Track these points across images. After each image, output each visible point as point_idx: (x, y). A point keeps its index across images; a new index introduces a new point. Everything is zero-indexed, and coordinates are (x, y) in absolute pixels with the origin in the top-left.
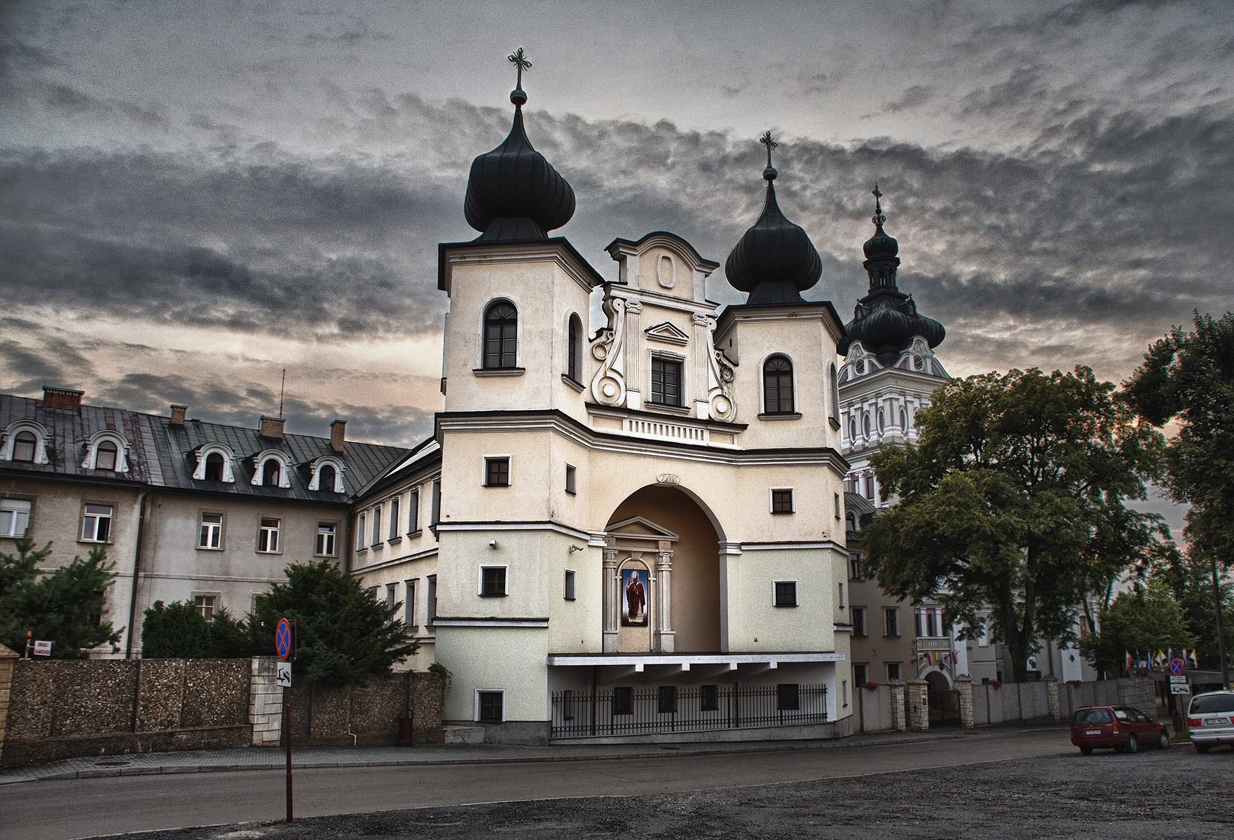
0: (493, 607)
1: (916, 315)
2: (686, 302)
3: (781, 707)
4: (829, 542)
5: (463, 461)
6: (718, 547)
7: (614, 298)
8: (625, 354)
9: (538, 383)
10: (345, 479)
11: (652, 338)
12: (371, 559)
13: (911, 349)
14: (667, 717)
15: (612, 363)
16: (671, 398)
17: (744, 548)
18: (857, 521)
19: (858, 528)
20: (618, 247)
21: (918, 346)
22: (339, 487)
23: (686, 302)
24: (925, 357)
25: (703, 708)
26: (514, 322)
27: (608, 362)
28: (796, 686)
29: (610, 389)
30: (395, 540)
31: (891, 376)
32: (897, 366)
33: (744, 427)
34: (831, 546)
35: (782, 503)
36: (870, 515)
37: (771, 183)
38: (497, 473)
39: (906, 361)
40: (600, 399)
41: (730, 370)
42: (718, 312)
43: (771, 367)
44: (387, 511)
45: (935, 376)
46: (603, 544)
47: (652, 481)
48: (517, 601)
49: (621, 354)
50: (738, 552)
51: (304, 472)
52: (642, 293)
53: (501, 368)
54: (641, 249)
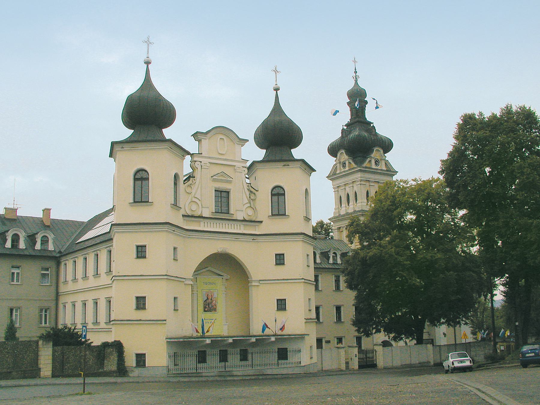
0: (141, 315)
1: (376, 134)
2: (231, 160)
3: (279, 358)
4: (303, 279)
5: (124, 245)
6: (249, 282)
7: (195, 161)
8: (201, 189)
9: (159, 209)
10: (54, 242)
11: (214, 180)
12: (71, 286)
13: (372, 156)
14: (223, 364)
15: (195, 195)
16: (224, 209)
17: (261, 282)
18: (339, 257)
19: (339, 261)
20: (197, 136)
21: (376, 153)
22: (51, 247)
23: (231, 160)
24: (381, 160)
25: (241, 360)
26: (147, 179)
27: (193, 194)
28: (287, 349)
29: (194, 207)
30: (85, 277)
31: (360, 171)
32: (364, 165)
33: (261, 222)
34: (303, 280)
35: (280, 259)
36: (346, 253)
37: (277, 92)
38: (141, 252)
39: (370, 161)
40: (190, 213)
41: (254, 194)
42: (248, 164)
43: (275, 192)
44: (80, 262)
45: (387, 171)
46: (191, 283)
47: (216, 251)
48: (152, 311)
49: (199, 191)
50: (257, 284)
51: (32, 239)
52: (209, 158)
53: (221, 192)
54: (208, 135)
